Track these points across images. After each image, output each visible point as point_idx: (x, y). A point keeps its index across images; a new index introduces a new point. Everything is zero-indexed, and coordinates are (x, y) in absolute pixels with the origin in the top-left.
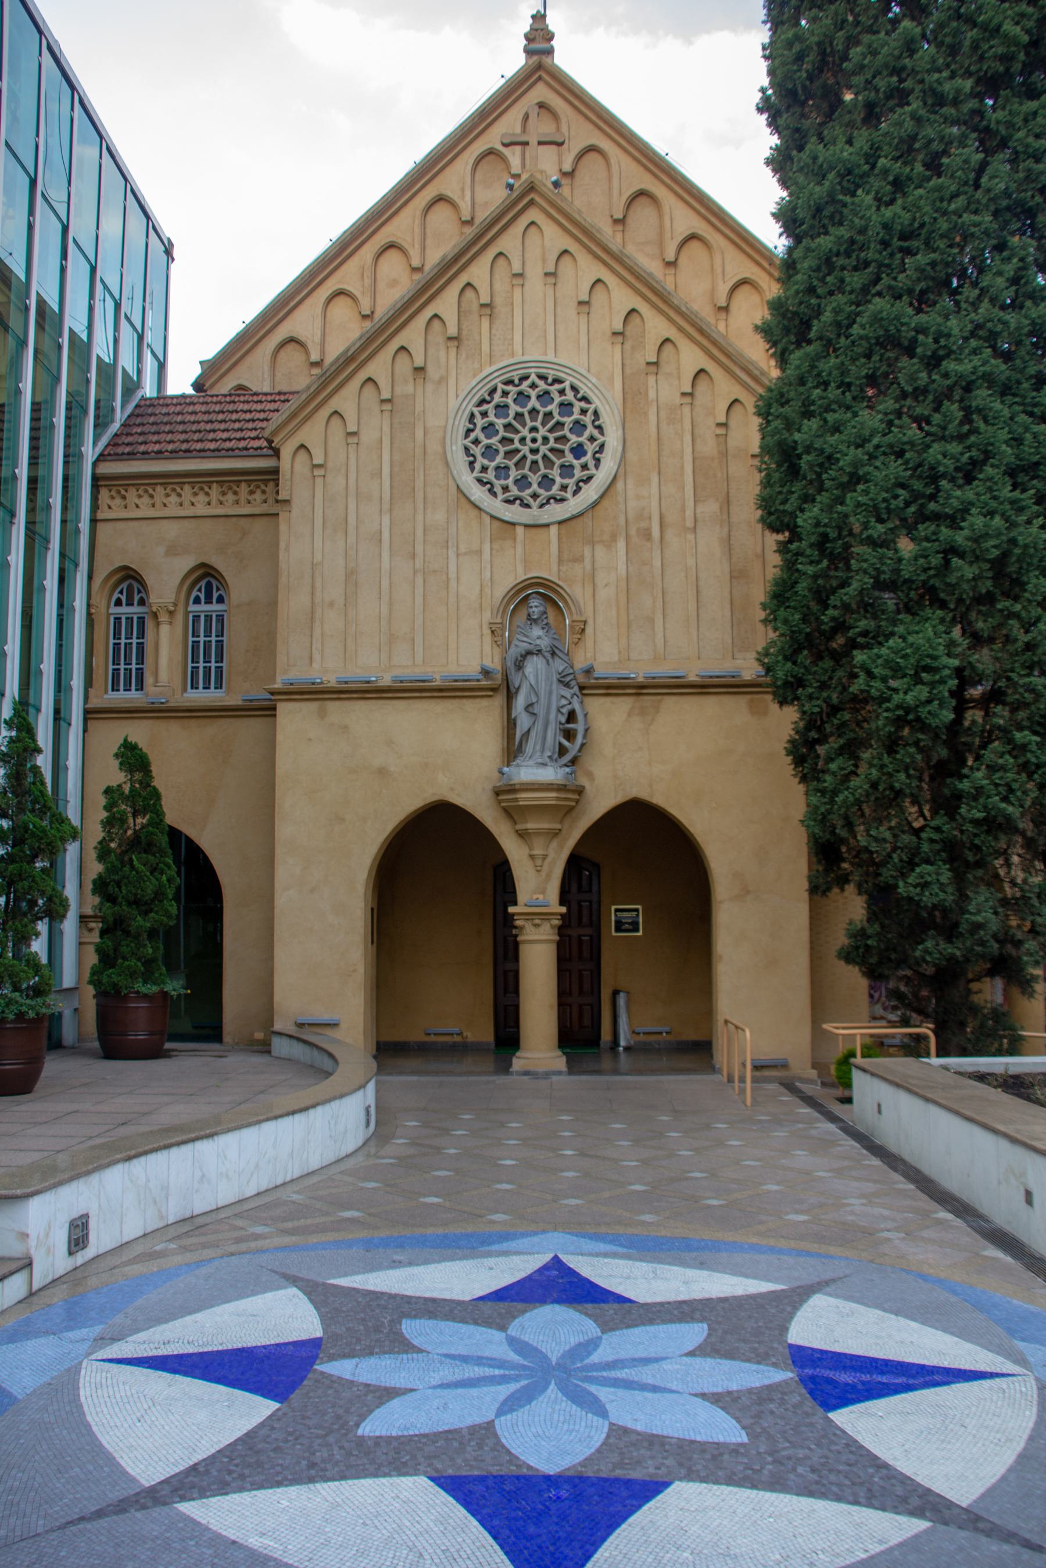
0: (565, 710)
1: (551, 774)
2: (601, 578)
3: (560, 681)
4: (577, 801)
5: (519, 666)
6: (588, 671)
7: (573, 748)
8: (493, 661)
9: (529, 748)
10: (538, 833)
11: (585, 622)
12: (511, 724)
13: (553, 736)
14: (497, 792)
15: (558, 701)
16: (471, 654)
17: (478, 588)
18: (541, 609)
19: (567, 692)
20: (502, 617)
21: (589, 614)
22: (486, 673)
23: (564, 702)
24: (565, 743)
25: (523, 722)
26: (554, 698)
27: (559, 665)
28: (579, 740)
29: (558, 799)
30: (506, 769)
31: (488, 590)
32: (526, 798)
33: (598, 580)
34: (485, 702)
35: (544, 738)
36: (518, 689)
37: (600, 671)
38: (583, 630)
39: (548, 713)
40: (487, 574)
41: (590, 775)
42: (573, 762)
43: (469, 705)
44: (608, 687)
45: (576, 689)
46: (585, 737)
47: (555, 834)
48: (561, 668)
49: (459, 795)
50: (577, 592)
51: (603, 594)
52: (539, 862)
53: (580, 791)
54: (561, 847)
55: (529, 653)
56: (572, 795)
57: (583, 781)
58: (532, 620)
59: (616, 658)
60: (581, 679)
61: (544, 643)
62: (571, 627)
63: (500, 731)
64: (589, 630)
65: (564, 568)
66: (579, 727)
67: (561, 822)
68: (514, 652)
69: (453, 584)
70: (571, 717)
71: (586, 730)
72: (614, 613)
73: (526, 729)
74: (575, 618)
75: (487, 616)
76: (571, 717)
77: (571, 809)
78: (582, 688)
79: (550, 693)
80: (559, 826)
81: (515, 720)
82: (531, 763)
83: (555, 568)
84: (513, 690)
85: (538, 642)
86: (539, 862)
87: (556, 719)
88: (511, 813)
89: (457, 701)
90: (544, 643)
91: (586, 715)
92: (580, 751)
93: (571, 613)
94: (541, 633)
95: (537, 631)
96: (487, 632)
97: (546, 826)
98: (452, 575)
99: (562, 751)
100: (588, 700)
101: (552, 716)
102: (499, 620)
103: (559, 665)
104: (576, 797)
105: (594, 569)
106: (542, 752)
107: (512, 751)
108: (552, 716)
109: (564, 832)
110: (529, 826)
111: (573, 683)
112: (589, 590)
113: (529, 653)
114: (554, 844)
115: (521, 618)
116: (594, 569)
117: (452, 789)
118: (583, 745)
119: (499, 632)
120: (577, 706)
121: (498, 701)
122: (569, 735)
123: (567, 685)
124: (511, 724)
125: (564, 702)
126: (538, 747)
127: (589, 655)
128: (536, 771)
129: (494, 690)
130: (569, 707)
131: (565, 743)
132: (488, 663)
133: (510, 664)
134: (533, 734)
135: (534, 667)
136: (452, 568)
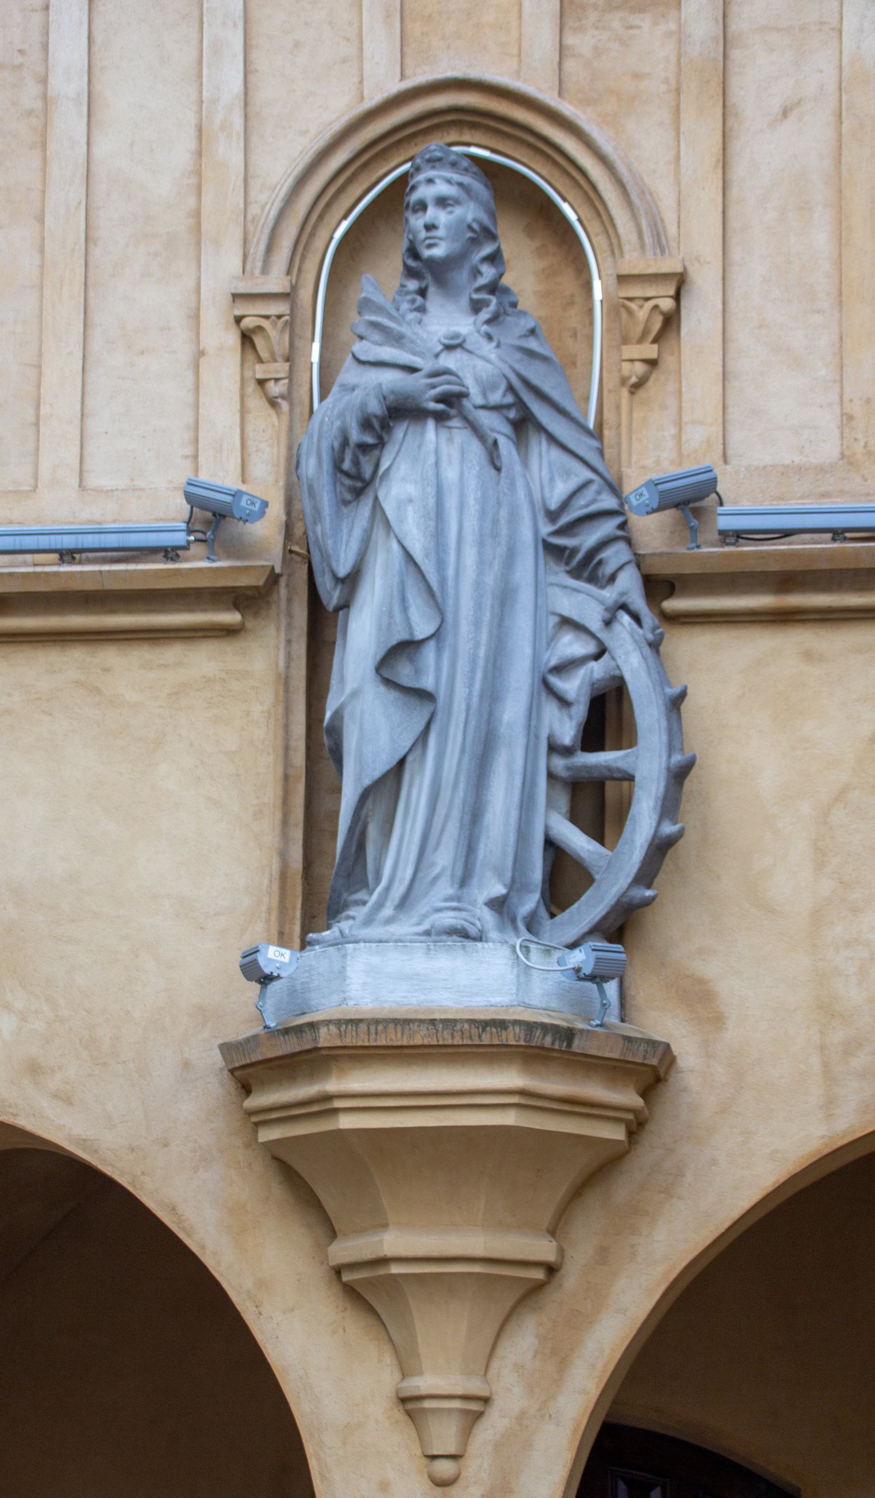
0: (574, 686)
1: (495, 978)
2: (763, 76)
3: (554, 551)
4: (636, 1126)
5: (356, 471)
6: (690, 500)
7: (614, 868)
8: (245, 455)
9: (396, 859)
10: (441, 1279)
11: (680, 283)
12: (322, 747)
13: (516, 808)
14: (249, 1070)
15: (542, 641)
16: (151, 432)
17: (187, 142)
18: (470, 212)
19: (585, 603)
20: (293, 267)
21: (696, 244)
22: (213, 518)
23: (572, 646)
24: (578, 841)
25: (372, 729)
26: (522, 624)
27: (549, 475)
28: (643, 823)
29: (528, 1100)
30: (276, 957)
31: (228, 152)
32: (370, 1096)
33: (744, 90)
34: (203, 661)
35: (475, 815)
36: (351, 582)
37: (742, 501)
38: (671, 322)
39: (492, 694)
40: (229, 79)
41: (699, 999)
42: (621, 926)
43: (128, 672)
44: (788, 580)
45: (629, 584)
46: (670, 806)
47: (529, 1288)
48: (560, 490)
49: (66, 1099)
50: (646, 148)
51: (773, 152)
52: (444, 1436)
53: (652, 1072)
54: (558, 1355)
55: (401, 411)
56: (611, 1093)
57: (662, 1022)
58: (427, 274)
59: (828, 450)
60: (653, 532)
61: (480, 369)
62: (617, 309)
63: (271, 794)
64: (699, 320)
65: (582, 42)
66: (645, 762)
67: (554, 1230)
68: (333, 415)
69: (69, 123)
70: (606, 716)
71: (679, 775)
72: (821, 238)
73: (380, 763)
74: (634, 261)
75: (223, 269)
76: (606, 716)
77: (602, 1168)
78: (657, 586)
79: (505, 598)
80: (543, 1249)
81: (336, 732)
82: (404, 928)
83: (542, 37)
84: (331, 596)
85: (448, 361)
86: (444, 1436)
87: (531, 727)
88: (313, 1177)
89: (78, 654)
90: (480, 369)
91: (676, 703)
92: (647, 874)
93: (615, 247)
94: (465, 325)
95: (447, 318)
96: (222, 339)
97: (475, 1243)
98: (68, 85)
99: (563, 879)
100: (691, 648)
101: (513, 711)
102: (276, 282)
103: (549, 475)
104: (628, 1097)
105: (726, 40)
106: (464, 880)
107: (325, 876)
108: (513, 711)
109: (571, 1278)
110: (393, 1242)
111: (615, 556)
112: (702, 133)
113: (401, 411)
114: (523, 1343)
115: (382, 279)
116: (726, 40)
117: (34, 1069)
118: (661, 849)
119: (275, 338)
120: (630, 659)
121: (269, 653)
122: (597, 804)
123: (587, 568)
124: (322, 747)
125: (572, 646)
126: (444, 858)
127: (697, 436)
128: (423, 964)
129: (251, 599)
130: (597, 670)
131: (578, 841)
132: (221, 475)
133: (315, 468)
134: (417, 792)
135: (423, 471)
136: (68, 50)
